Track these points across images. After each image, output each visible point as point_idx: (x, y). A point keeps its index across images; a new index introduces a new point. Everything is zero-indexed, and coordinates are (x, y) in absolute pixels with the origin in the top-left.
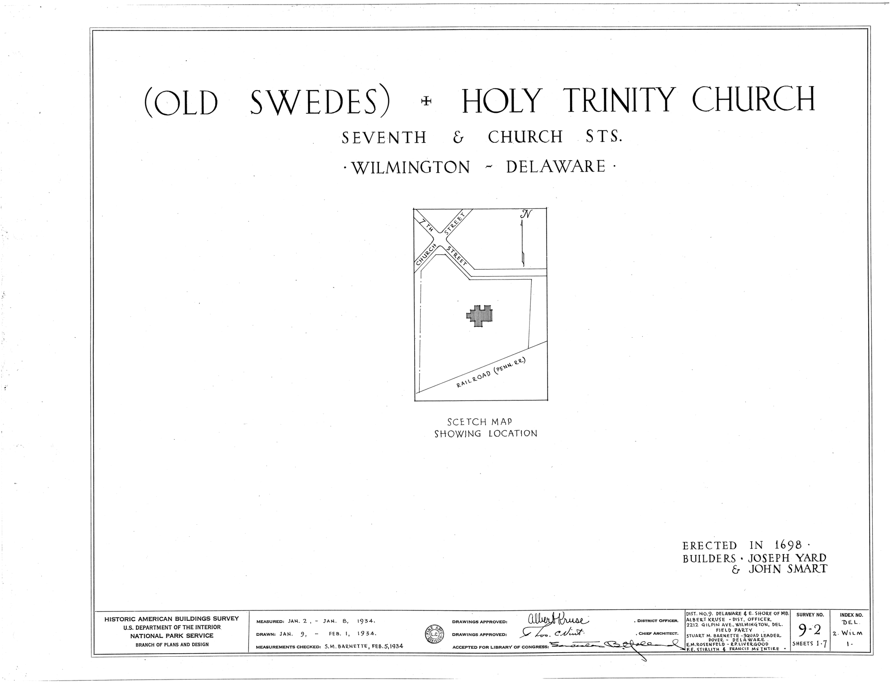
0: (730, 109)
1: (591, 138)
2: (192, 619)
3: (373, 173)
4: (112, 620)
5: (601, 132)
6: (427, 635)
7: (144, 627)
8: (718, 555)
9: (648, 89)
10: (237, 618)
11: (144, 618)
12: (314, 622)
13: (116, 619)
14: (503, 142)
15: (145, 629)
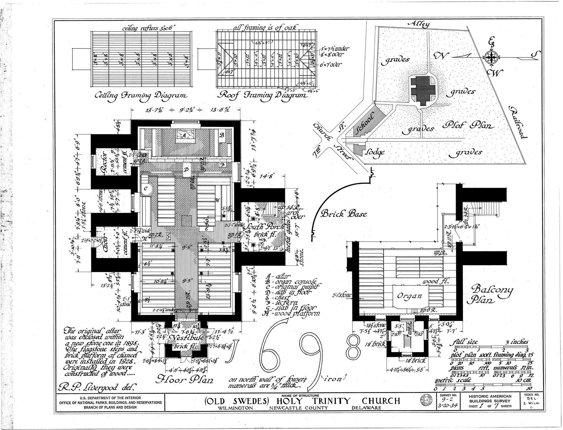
1: (364, 399)
2: (480, 401)
4: (473, 397)
6: (422, 400)
7: (93, 398)
10: (509, 401)
11: (494, 396)
12: (490, 114)
13: (476, 396)
15: (94, 399)
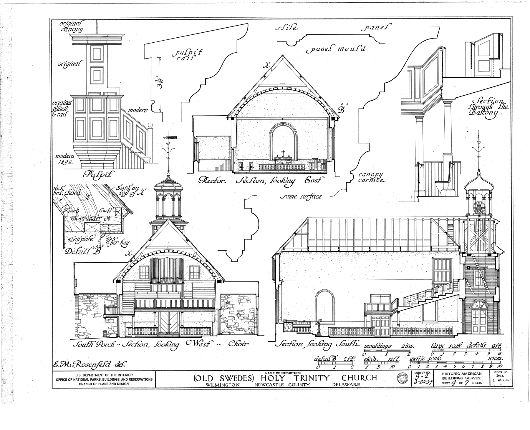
0: (204, 376)
2: (453, 378)
9: (320, 376)
10: (479, 378)
11: (480, 373)
12: (304, 140)
13: (449, 374)
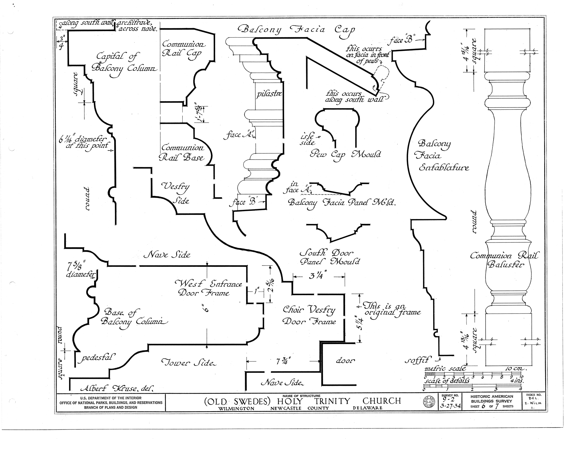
3: (336, 399)
5: (340, 399)
6: (424, 402)
7: (93, 398)
8: (260, 399)
10: (511, 401)
11: (495, 396)
13: (478, 396)
14: (396, 403)
